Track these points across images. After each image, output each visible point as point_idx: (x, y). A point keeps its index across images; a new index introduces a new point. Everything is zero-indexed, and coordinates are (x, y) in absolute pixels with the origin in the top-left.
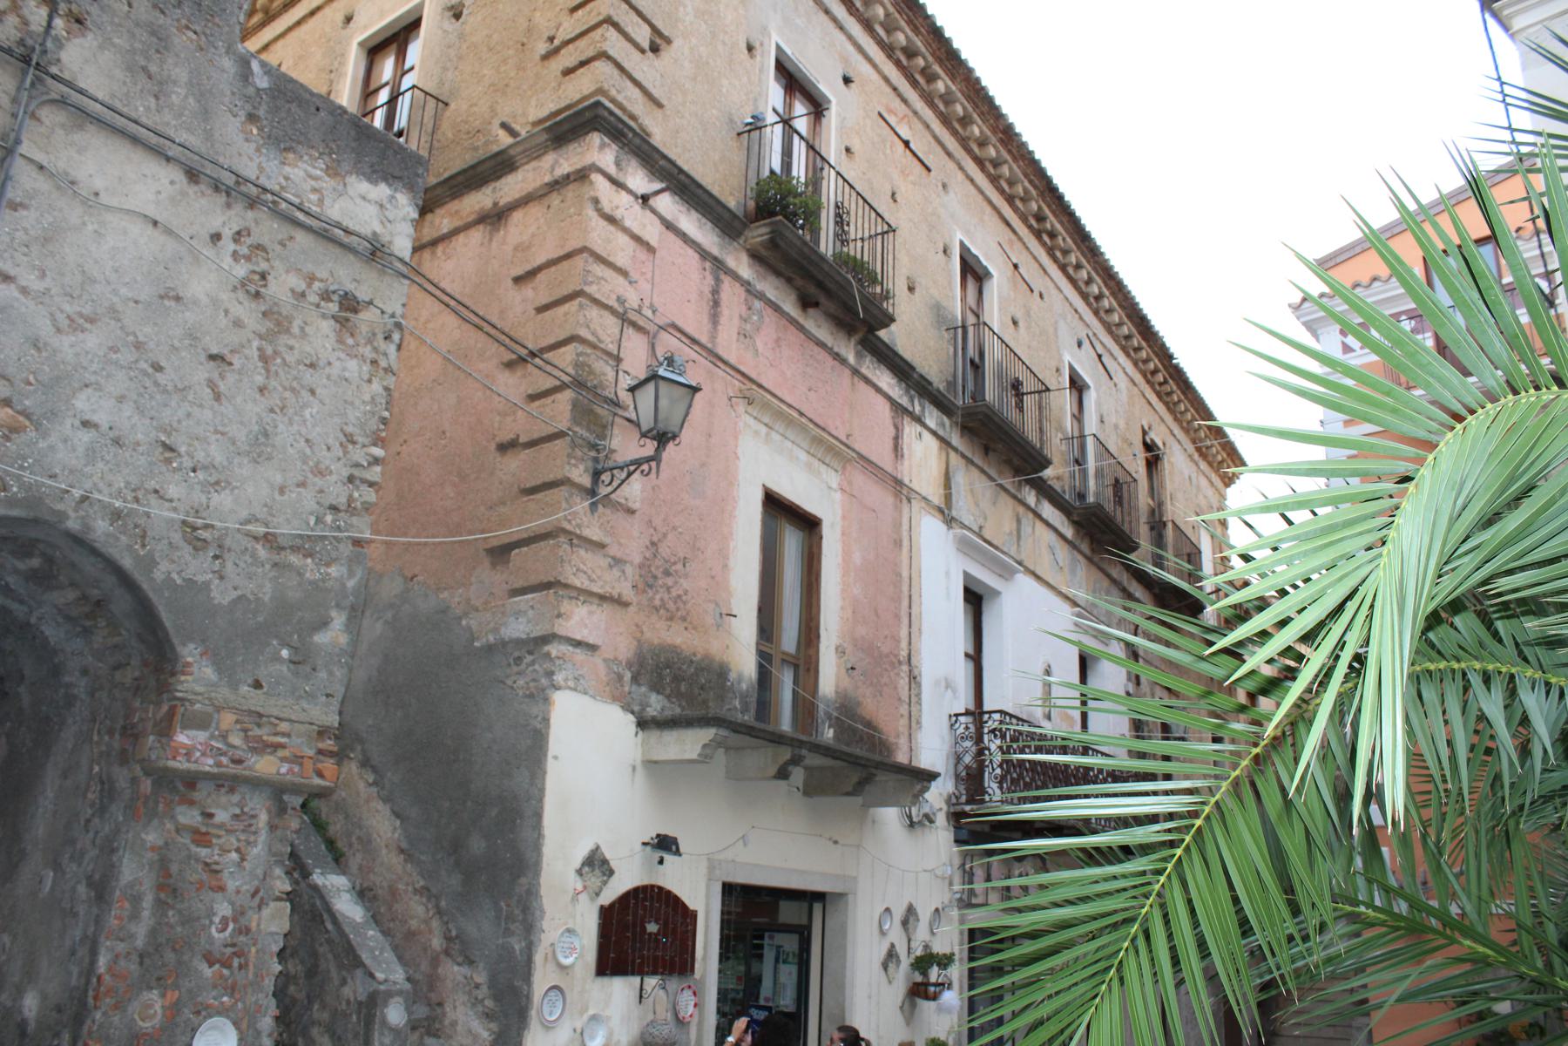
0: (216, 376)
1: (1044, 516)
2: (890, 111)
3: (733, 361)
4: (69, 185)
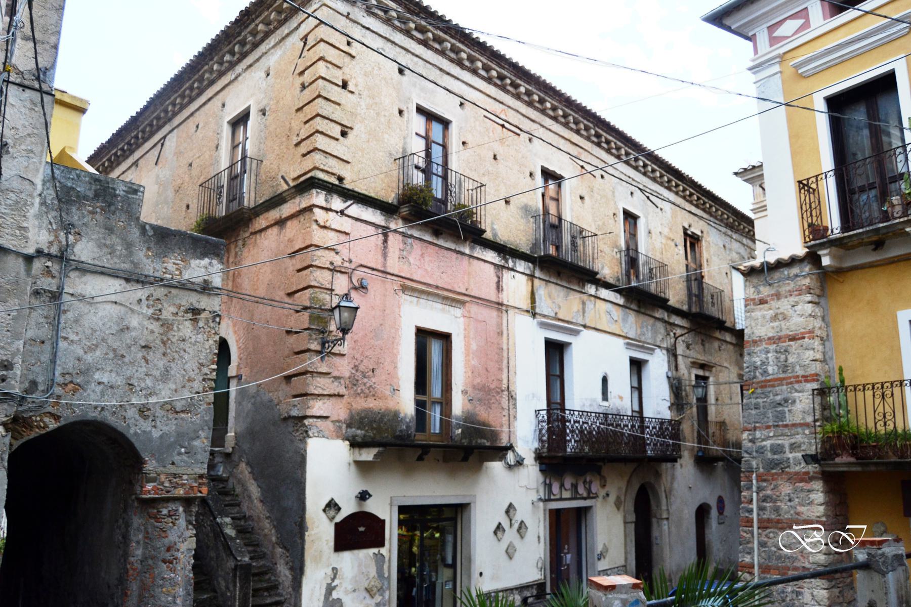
0: (145, 353)
3: (396, 273)
4: (82, 298)
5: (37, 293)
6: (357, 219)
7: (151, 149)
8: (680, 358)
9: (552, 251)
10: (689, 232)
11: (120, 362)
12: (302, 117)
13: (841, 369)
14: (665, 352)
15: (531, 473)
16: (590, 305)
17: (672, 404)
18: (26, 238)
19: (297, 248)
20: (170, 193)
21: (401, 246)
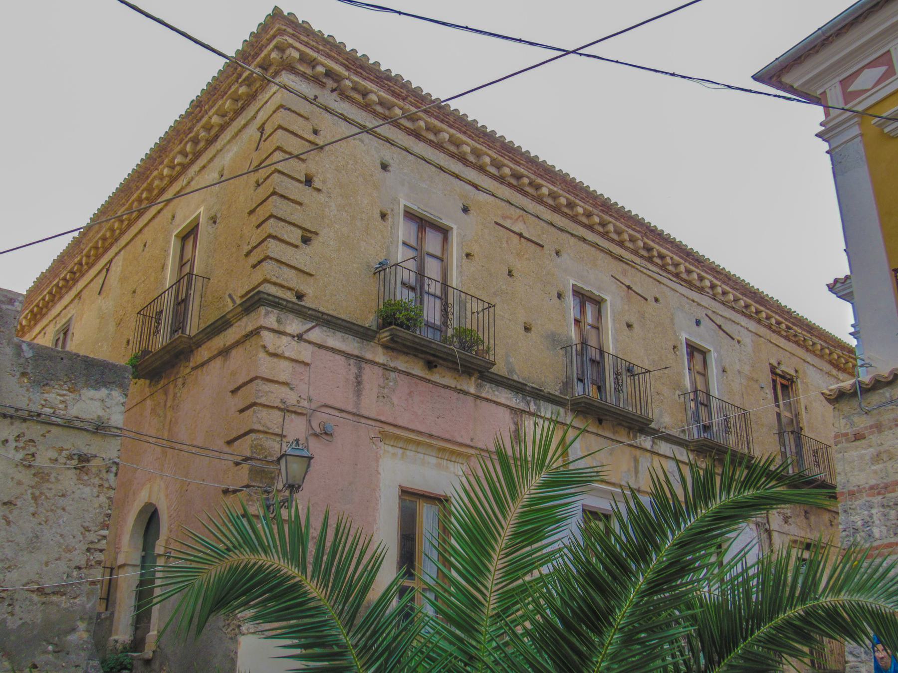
0: (7, 513)
1: (661, 452)
2: (505, 217)
3: (372, 415)
6: (320, 346)
8: (775, 535)
10: (778, 371)
19: (240, 382)
20: (111, 327)
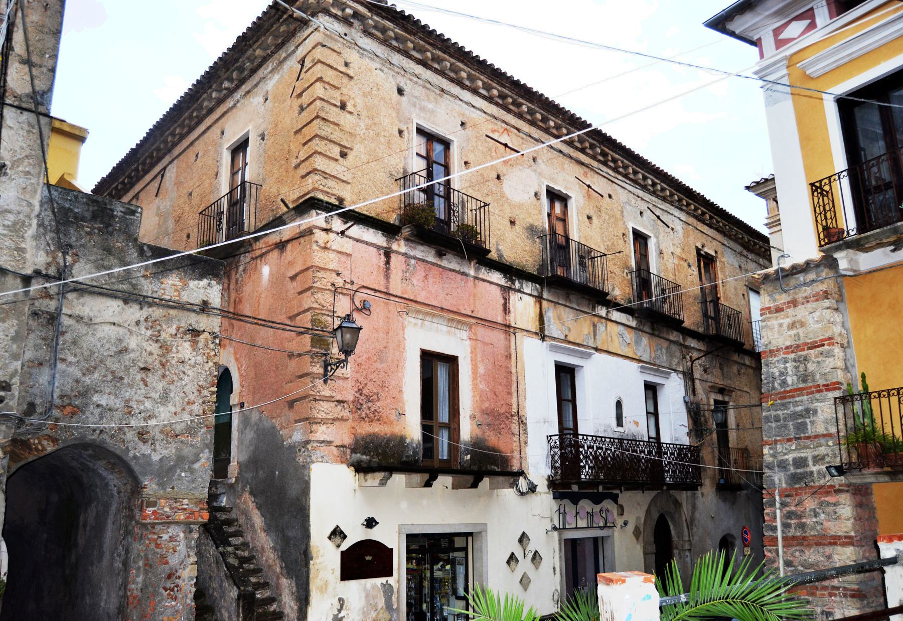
0: (144, 376)
1: (613, 319)
2: (493, 131)
3: (399, 295)
4: (79, 319)
5: (35, 314)
6: (358, 241)
7: (151, 181)
8: (697, 382)
9: (559, 272)
11: (118, 384)
12: (301, 138)
13: (863, 376)
14: (681, 376)
15: (544, 502)
16: (601, 328)
17: (690, 431)
18: (24, 259)
20: (171, 224)
21: (404, 267)
